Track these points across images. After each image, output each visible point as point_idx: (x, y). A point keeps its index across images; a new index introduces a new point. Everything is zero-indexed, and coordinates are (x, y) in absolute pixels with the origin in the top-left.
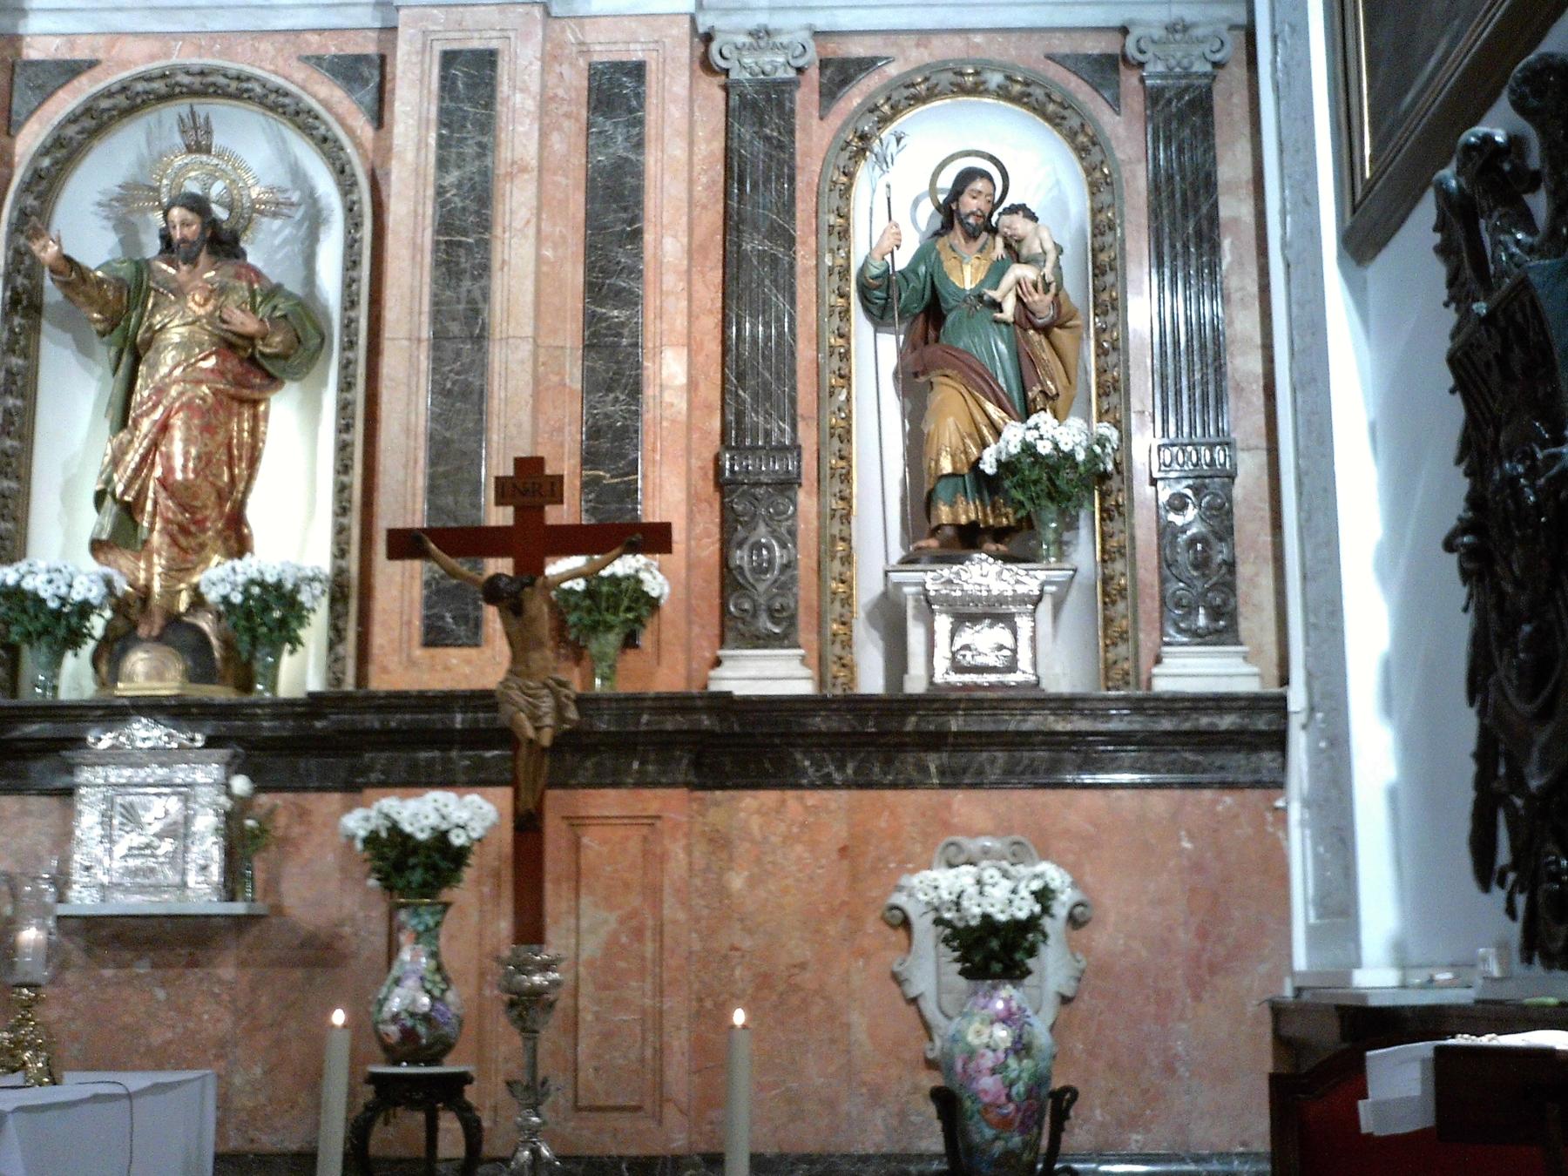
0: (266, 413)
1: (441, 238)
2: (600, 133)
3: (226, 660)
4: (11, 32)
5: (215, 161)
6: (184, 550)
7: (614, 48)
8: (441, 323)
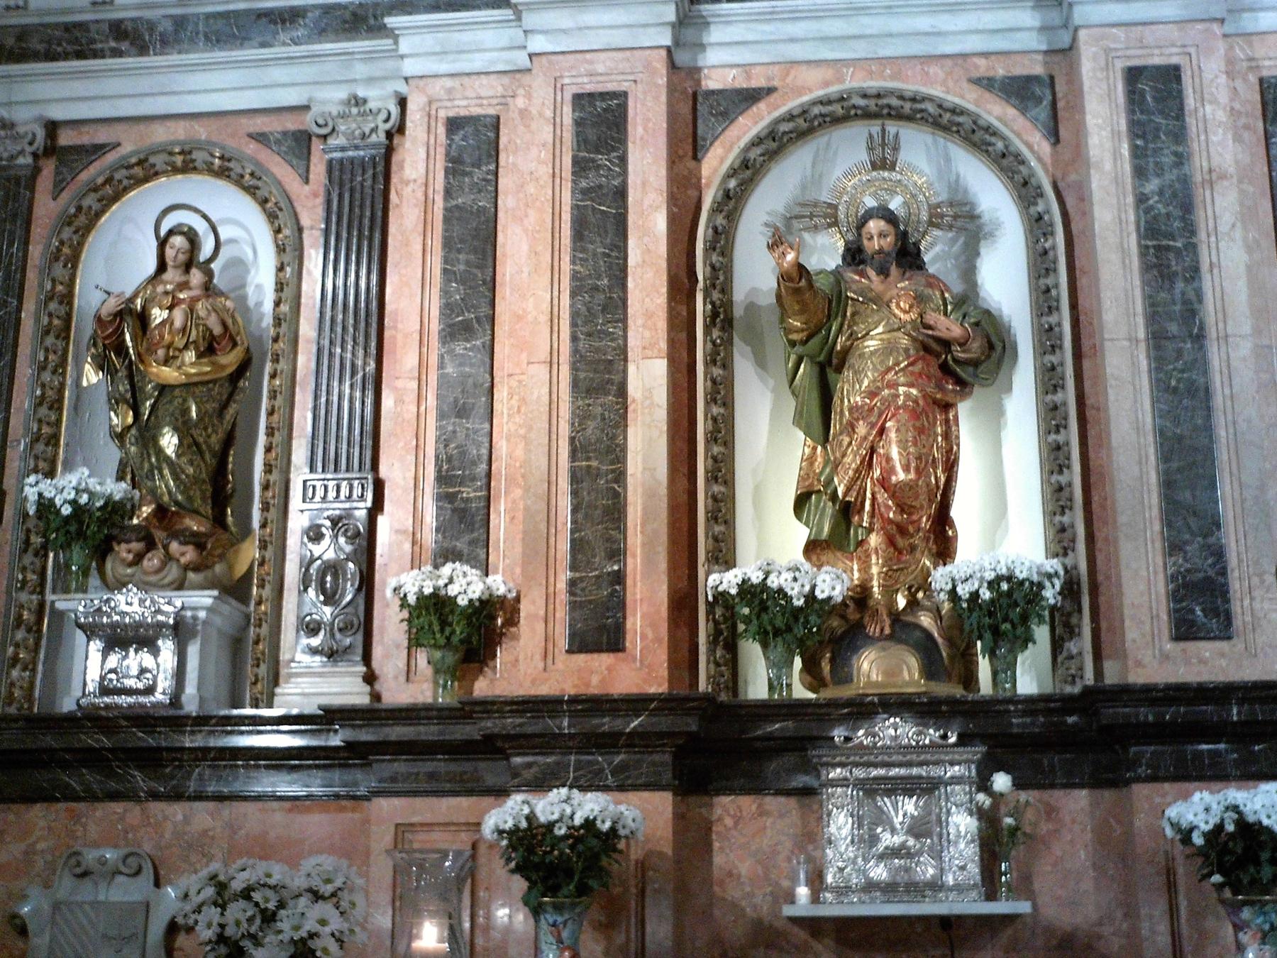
0: (956, 418)
1: (1150, 243)
3: (951, 657)
4: (692, 64)
5: (899, 177)
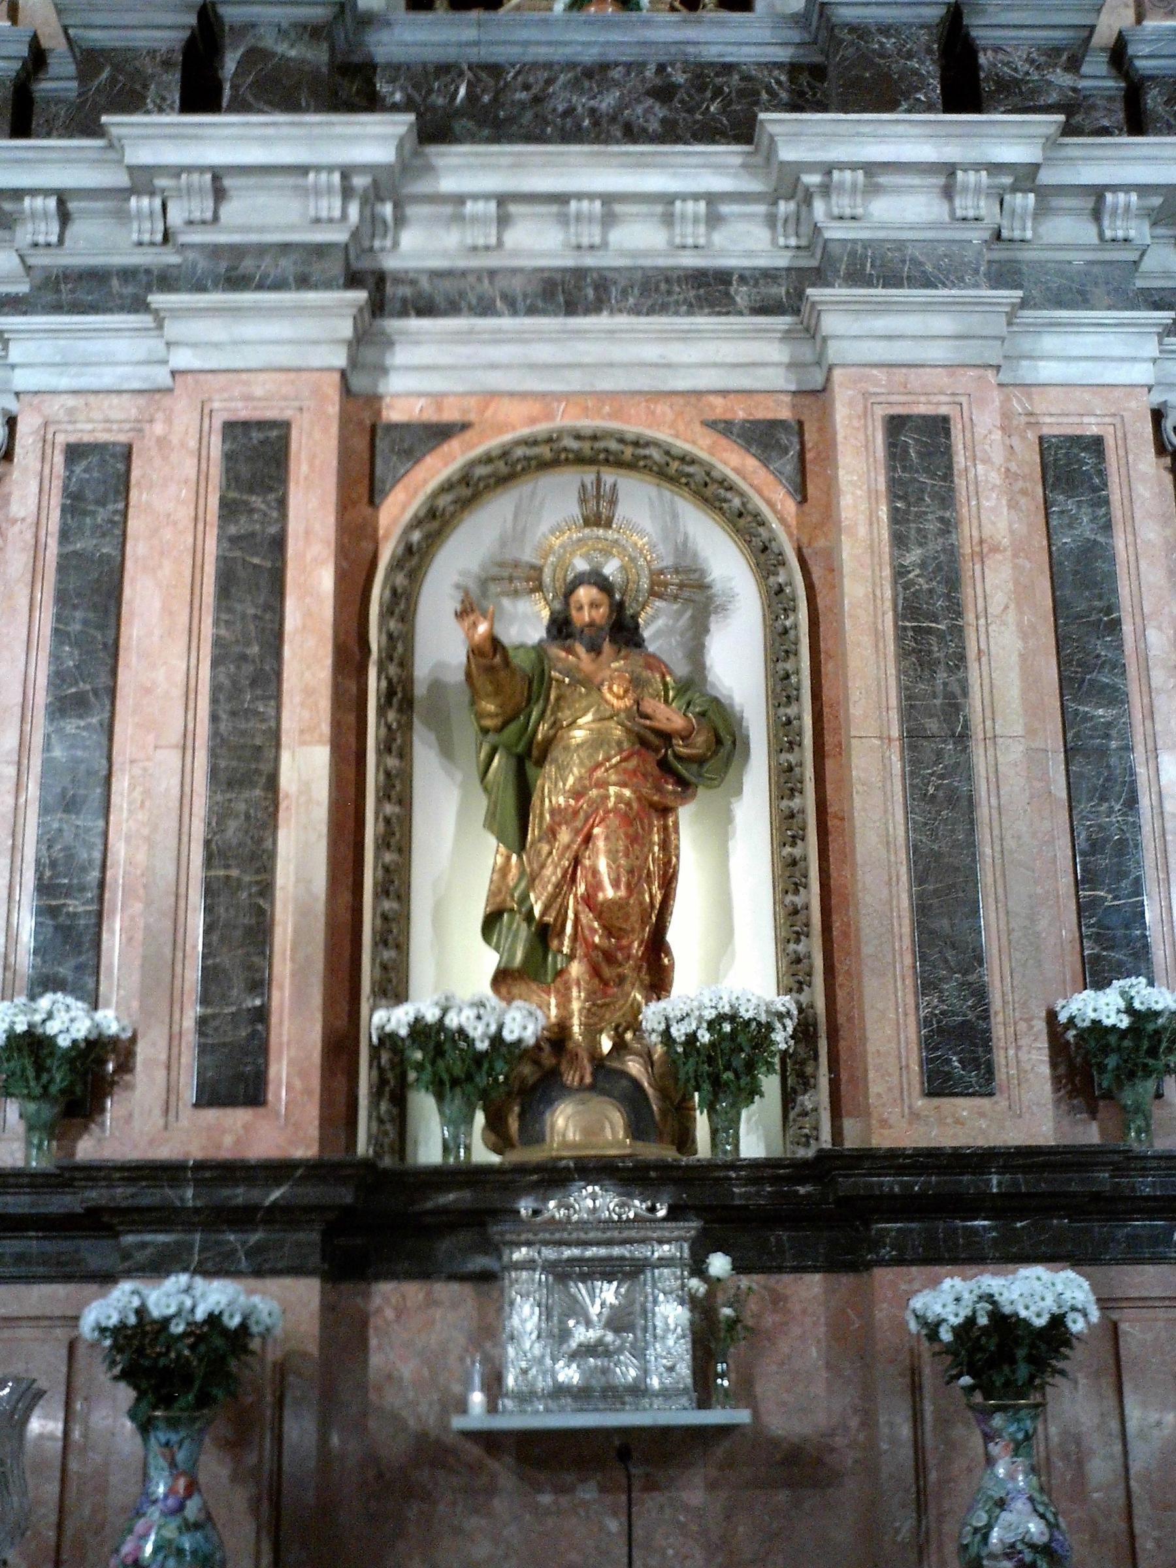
2: (1062, 512)
3: (663, 1112)
6: (605, 983)
7: (1065, 420)
8: (916, 719)
